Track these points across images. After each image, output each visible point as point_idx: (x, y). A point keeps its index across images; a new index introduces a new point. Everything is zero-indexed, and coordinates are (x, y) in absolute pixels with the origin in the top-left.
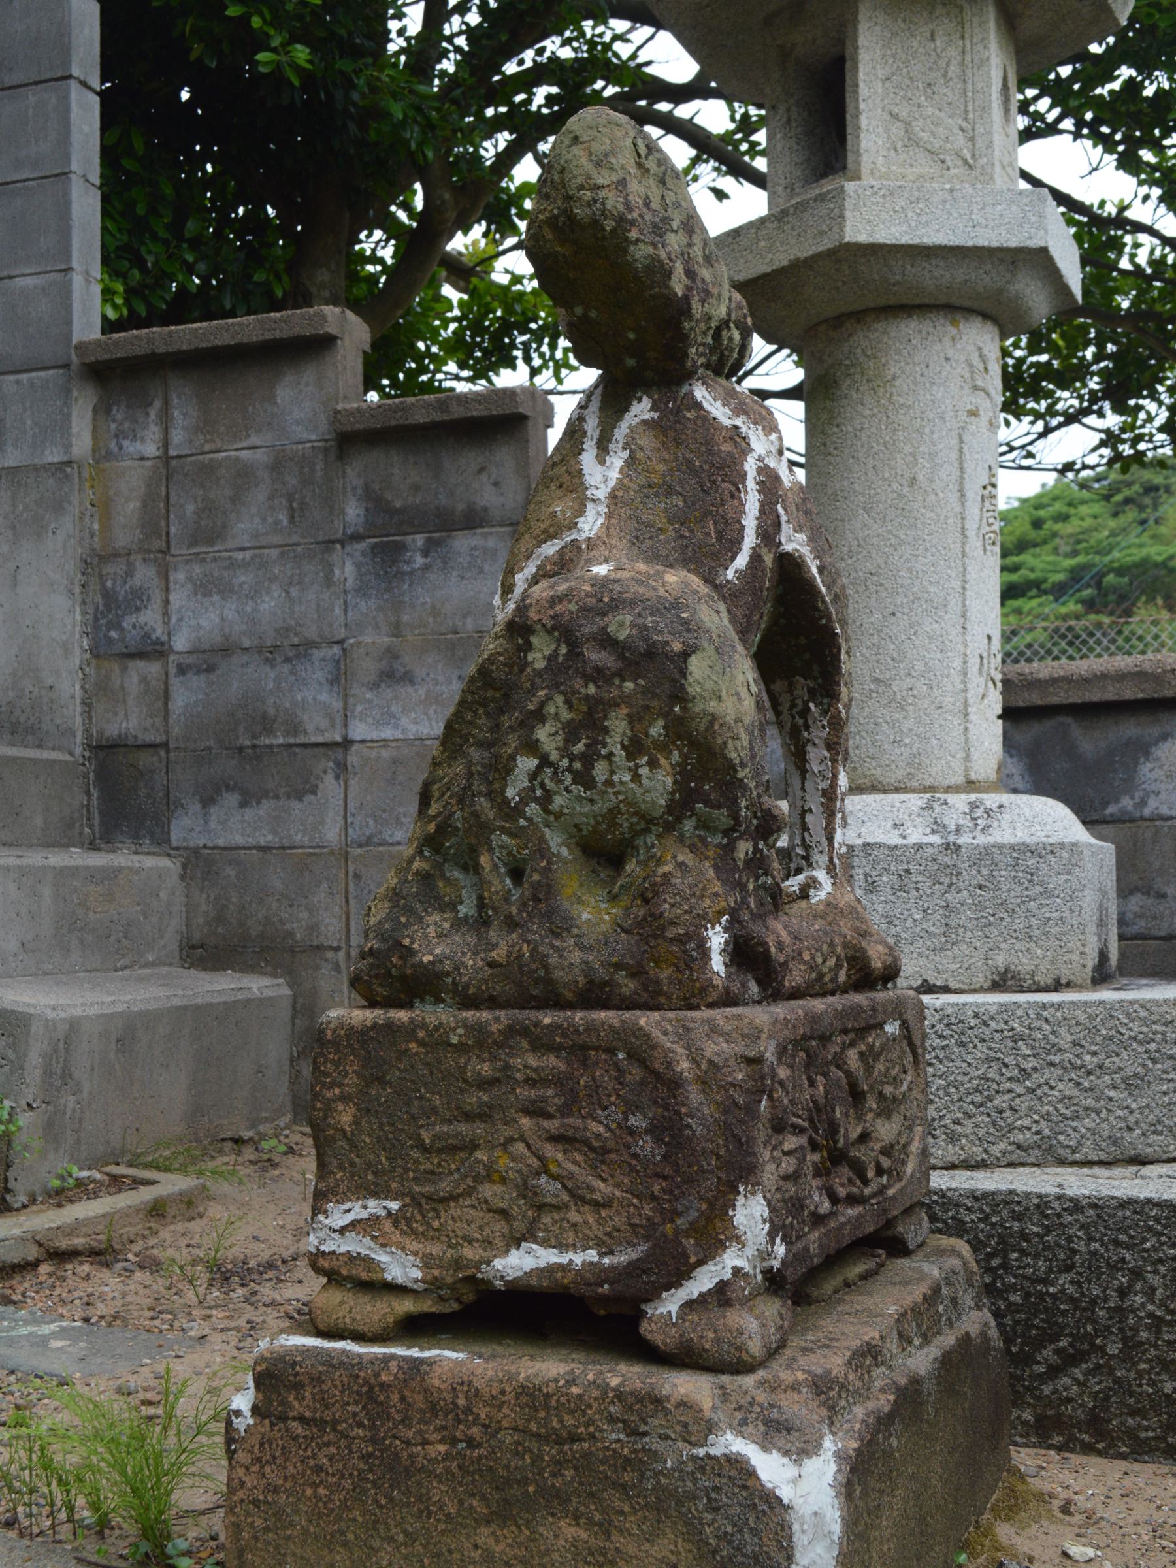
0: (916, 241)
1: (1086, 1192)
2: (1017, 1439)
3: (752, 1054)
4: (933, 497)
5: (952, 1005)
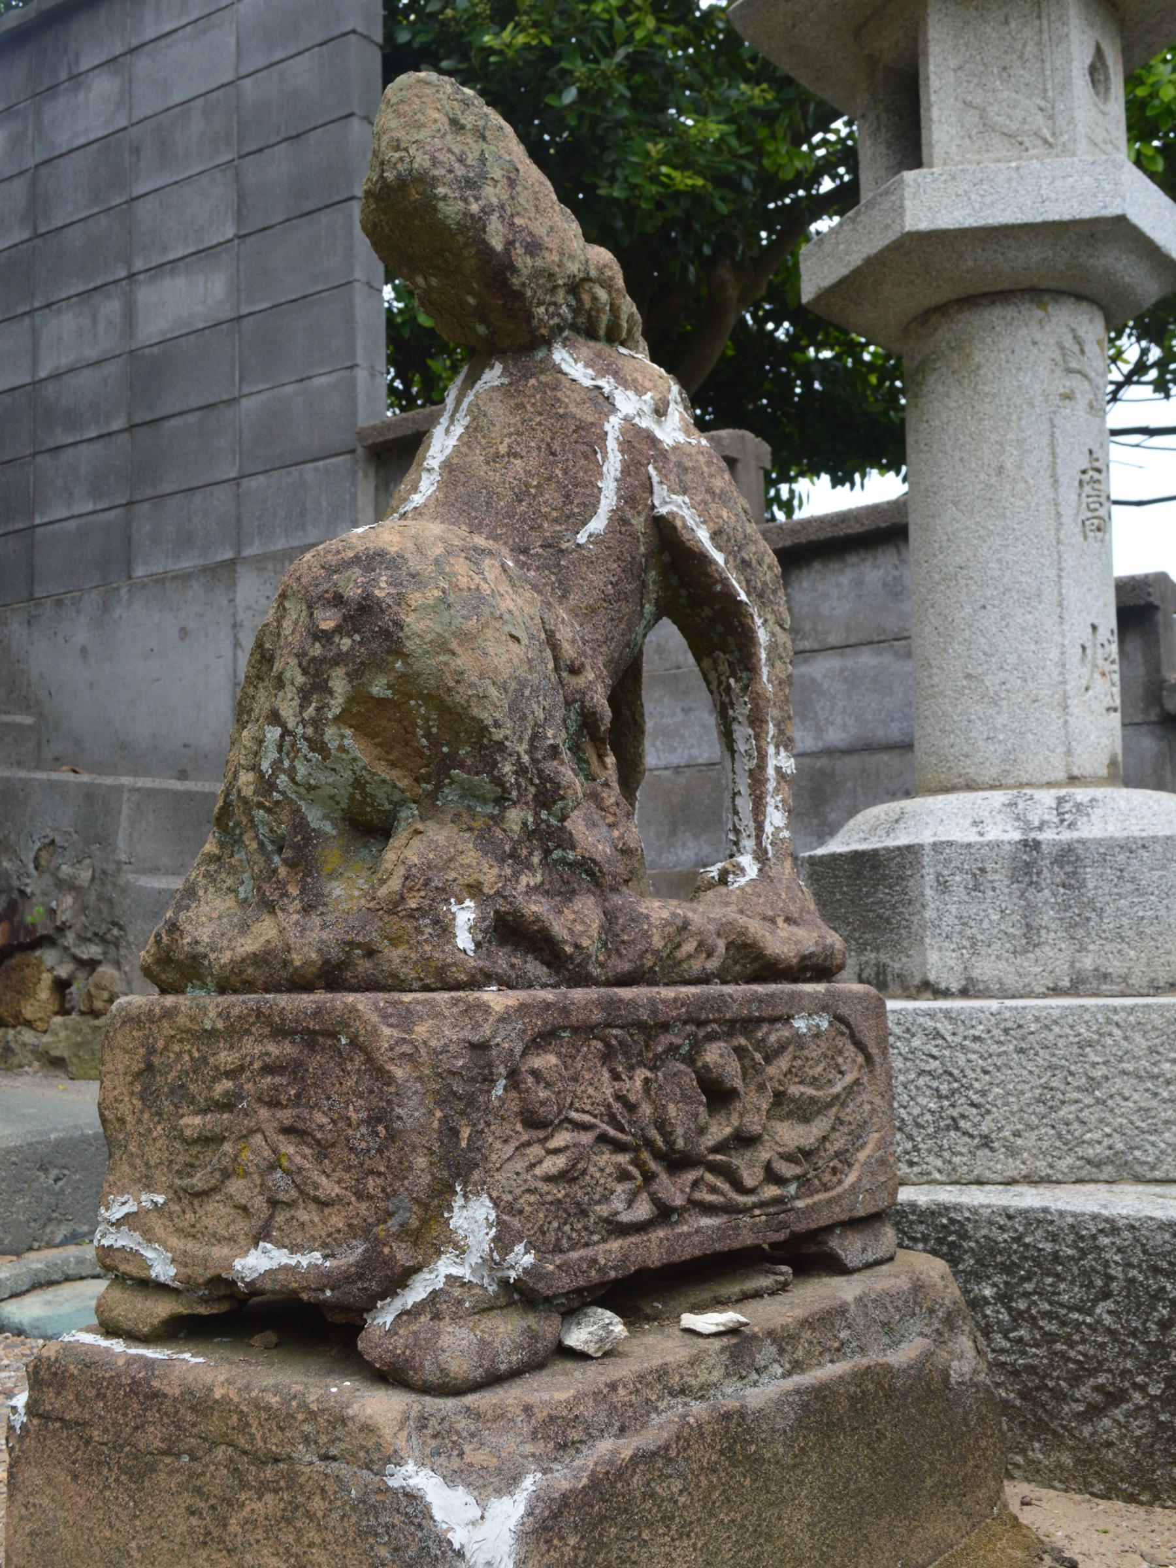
0: (981, 223)
1: (1124, 1212)
2: (1056, 1483)
3: (475, 1039)
4: (1022, 485)
5: (1010, 1009)
